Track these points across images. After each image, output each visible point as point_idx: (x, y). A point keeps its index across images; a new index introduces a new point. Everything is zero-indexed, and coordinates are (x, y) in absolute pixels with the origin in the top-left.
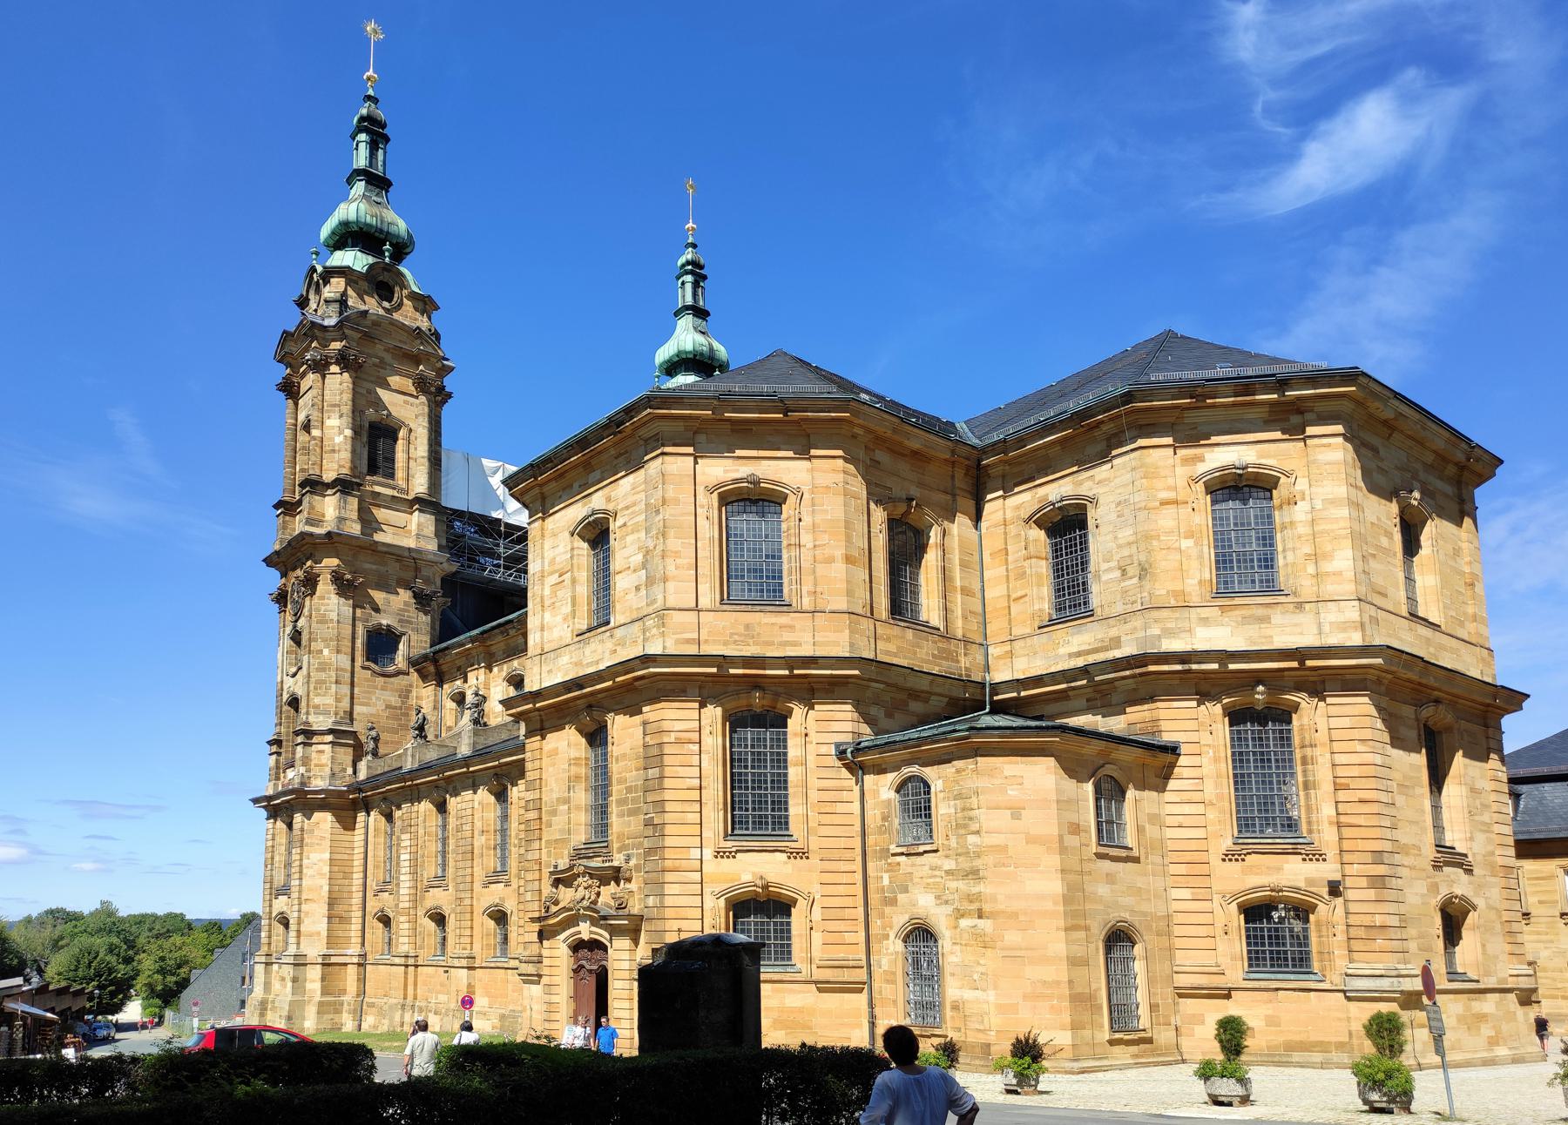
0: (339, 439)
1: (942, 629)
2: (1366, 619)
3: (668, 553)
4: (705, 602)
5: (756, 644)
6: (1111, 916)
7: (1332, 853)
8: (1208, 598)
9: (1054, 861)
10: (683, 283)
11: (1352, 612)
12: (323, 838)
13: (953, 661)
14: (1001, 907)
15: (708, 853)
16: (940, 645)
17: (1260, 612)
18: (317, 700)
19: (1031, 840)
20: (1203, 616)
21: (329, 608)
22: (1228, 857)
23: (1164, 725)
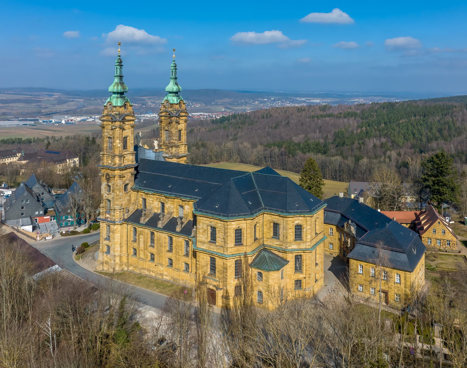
18: (116, 203)
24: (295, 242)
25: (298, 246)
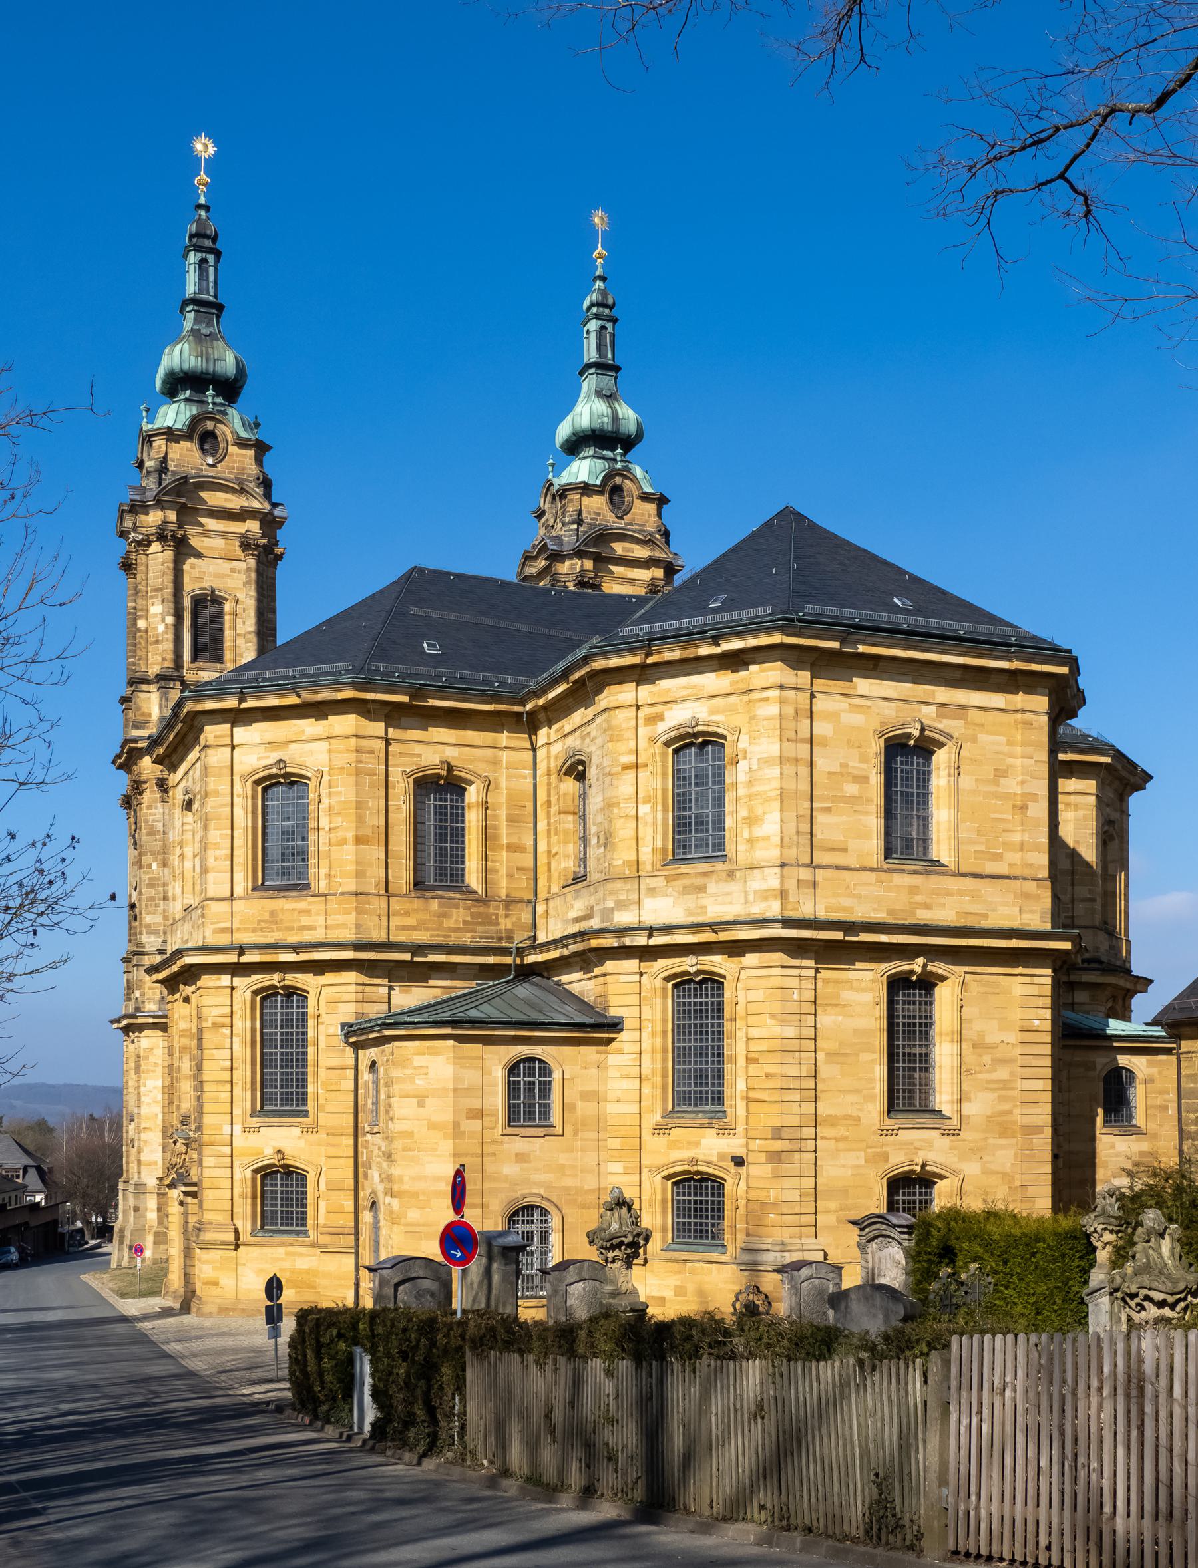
0: (161, 628)
1: (480, 893)
2: (791, 885)
3: (209, 845)
4: (239, 891)
5: (279, 930)
6: (519, 1193)
7: (740, 1129)
8: (659, 867)
9: (447, 1146)
10: (588, 332)
11: (772, 880)
12: (156, 1065)
13: (490, 924)
14: (406, 1187)
15: (238, 1128)
16: (474, 910)
17: (699, 881)
19: (432, 1126)
20: (651, 886)
21: (156, 818)
22: (657, 1130)
23: (612, 1000)
24: (672, 870)
25: (690, 901)
